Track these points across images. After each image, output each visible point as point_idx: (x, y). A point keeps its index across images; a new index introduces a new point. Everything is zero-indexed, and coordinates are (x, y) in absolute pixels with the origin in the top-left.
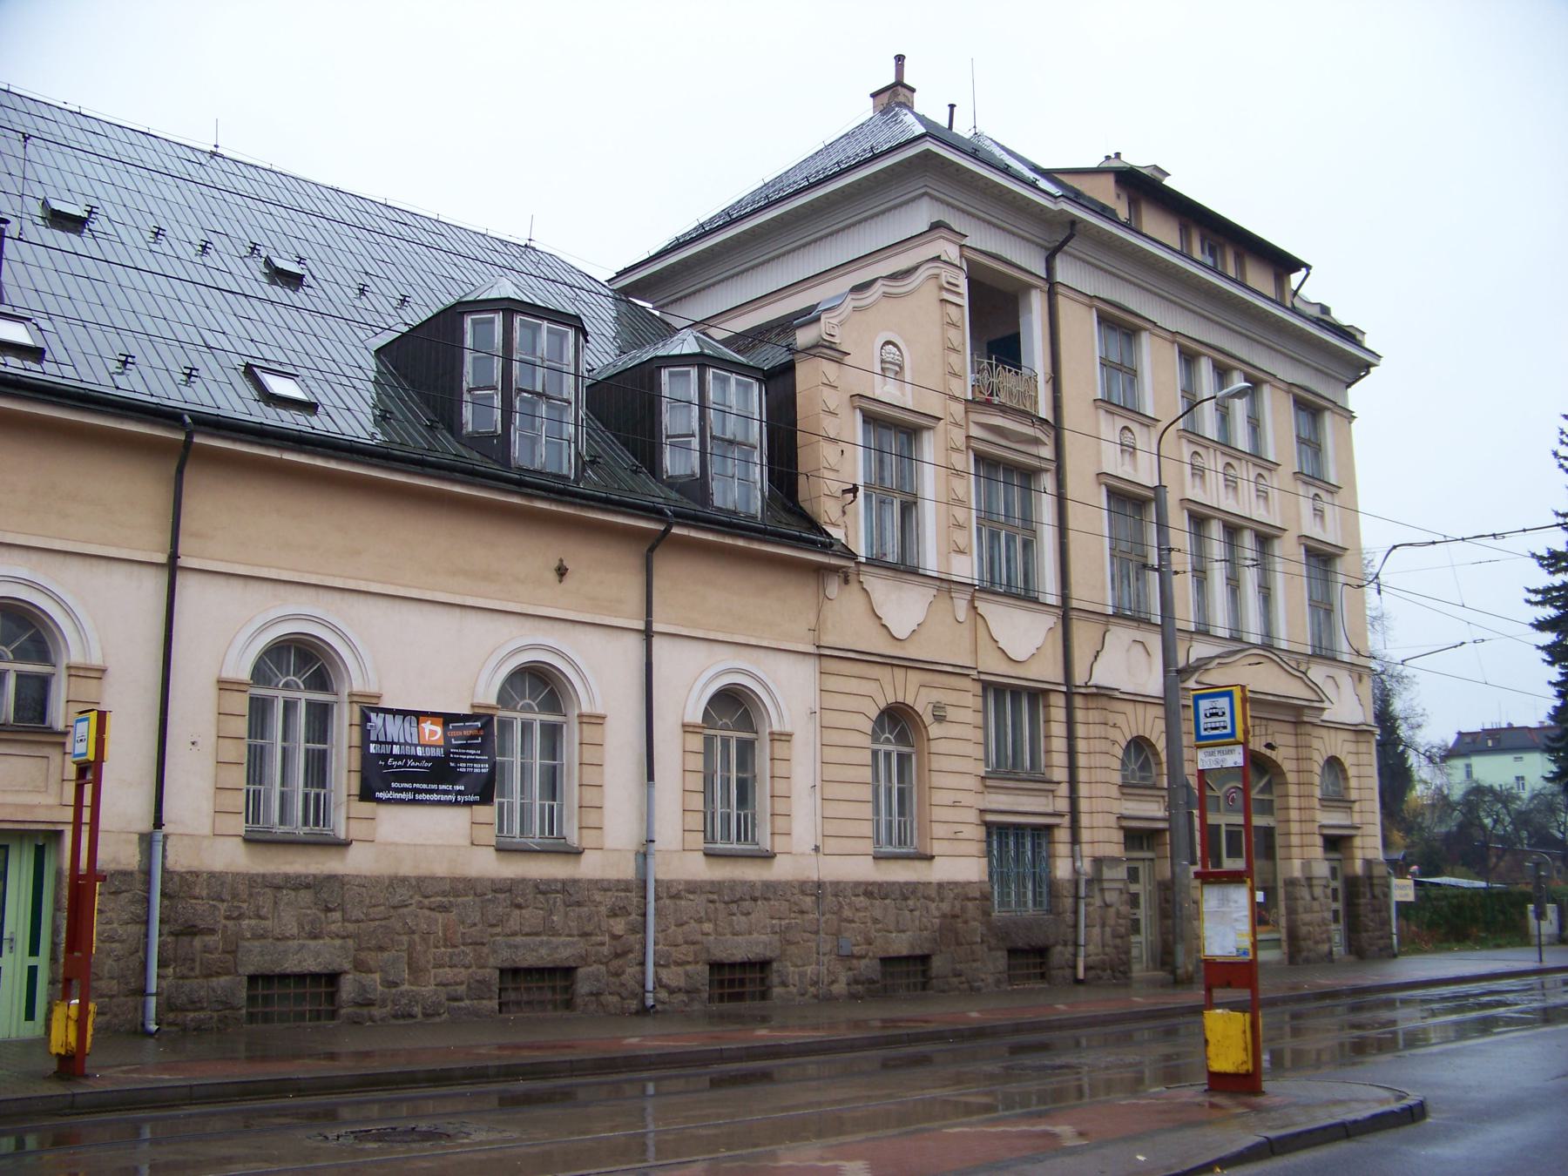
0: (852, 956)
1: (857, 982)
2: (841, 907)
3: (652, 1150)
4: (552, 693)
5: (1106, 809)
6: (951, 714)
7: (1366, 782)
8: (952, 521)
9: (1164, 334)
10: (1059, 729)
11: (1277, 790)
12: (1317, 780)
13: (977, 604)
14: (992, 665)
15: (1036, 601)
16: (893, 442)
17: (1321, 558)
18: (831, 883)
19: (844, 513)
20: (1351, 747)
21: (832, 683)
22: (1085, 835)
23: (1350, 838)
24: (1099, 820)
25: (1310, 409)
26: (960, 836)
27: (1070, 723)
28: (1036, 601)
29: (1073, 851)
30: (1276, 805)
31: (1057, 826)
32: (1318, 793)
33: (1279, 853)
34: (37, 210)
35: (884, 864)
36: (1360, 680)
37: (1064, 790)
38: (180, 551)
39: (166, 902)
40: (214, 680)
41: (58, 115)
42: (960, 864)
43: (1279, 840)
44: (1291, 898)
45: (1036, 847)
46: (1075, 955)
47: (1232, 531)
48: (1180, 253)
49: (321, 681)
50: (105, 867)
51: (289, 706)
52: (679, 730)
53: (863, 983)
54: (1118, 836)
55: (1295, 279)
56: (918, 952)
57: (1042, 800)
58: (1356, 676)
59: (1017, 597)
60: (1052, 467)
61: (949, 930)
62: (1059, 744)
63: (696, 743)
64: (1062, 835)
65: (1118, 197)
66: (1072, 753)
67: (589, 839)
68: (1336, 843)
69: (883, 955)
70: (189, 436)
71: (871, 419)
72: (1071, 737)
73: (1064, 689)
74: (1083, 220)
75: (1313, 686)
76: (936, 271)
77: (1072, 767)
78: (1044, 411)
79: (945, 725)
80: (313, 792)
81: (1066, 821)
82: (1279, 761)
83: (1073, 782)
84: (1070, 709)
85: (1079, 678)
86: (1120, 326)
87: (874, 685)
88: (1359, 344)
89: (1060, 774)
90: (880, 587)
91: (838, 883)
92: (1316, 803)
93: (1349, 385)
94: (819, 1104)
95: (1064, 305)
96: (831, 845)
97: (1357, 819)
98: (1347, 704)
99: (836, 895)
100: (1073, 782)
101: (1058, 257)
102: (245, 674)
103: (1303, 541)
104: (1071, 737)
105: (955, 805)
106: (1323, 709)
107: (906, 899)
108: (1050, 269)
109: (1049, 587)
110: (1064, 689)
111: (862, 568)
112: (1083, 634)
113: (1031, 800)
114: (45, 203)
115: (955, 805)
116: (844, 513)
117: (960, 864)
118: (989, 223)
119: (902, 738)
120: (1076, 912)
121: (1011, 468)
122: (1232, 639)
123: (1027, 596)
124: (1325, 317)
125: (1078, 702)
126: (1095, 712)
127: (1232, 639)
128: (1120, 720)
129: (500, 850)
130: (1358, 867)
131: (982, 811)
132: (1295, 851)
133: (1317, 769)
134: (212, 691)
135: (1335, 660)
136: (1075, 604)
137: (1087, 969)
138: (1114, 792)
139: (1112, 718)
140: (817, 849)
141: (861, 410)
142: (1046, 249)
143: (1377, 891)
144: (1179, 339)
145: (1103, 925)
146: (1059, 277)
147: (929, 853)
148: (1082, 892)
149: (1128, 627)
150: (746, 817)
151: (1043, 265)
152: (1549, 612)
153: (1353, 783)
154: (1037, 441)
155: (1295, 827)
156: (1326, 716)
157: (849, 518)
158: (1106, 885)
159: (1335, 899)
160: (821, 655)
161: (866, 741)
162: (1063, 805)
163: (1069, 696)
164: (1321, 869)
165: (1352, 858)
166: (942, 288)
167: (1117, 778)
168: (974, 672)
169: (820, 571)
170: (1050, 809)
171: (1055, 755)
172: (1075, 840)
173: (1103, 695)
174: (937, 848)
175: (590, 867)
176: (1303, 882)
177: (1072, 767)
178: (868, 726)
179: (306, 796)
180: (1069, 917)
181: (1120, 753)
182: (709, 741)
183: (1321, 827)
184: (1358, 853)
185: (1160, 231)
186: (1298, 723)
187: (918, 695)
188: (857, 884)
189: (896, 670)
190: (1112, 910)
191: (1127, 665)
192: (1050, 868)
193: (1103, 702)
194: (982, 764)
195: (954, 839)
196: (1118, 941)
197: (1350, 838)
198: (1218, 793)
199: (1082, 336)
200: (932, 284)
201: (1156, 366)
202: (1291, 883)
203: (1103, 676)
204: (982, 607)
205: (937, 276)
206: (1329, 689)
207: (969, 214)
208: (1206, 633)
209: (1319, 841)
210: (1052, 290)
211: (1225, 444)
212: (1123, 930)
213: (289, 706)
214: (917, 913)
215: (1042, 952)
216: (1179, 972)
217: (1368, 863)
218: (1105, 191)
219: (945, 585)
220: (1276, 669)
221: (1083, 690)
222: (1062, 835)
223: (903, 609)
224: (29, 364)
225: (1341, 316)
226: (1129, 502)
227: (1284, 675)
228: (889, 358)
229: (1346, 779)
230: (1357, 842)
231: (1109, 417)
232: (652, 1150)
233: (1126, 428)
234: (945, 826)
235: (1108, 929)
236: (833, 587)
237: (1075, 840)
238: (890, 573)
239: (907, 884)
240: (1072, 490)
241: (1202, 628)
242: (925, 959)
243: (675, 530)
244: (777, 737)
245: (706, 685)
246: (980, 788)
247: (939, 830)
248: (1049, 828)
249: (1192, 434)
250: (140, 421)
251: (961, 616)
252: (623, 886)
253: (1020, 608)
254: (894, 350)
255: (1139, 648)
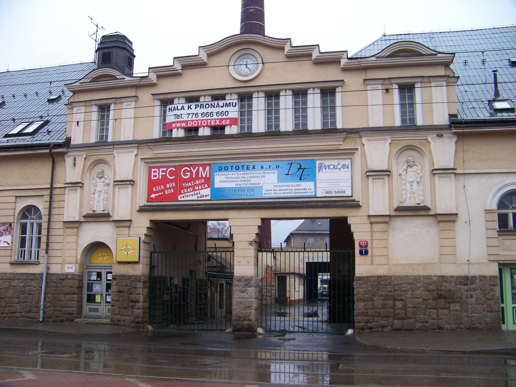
3: (39, 364)
34: (507, 63)
40: (483, 209)
41: (511, 30)
50: (77, 270)
51: (32, 224)
80: (37, 249)
94: (373, 371)
102: (494, 207)
114: (509, 60)
134: (483, 214)
179: (35, 251)
213: (32, 224)
224: (510, 114)
232: (39, 364)
243: (48, 151)
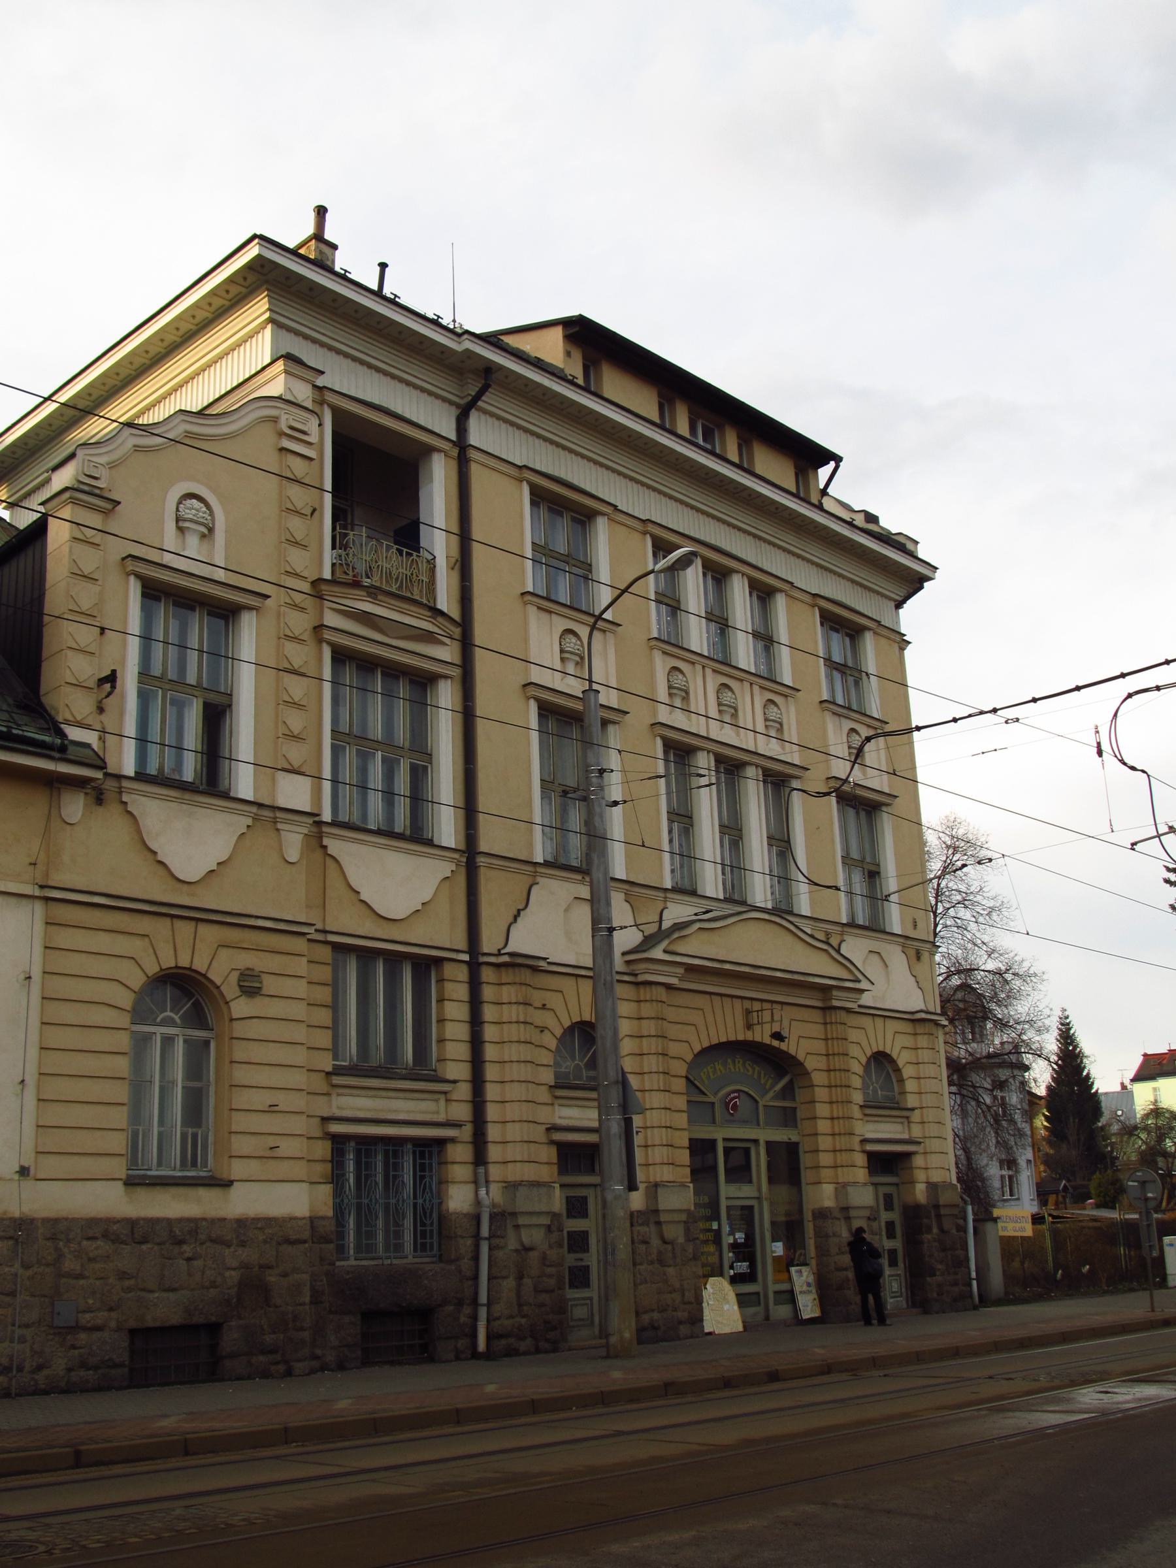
0: (76, 1328)
1: (84, 1365)
2: (60, 1256)
4: (197, 1006)
5: (527, 1114)
6: (270, 985)
7: (931, 1085)
8: (282, 730)
9: (630, 521)
10: (457, 1011)
11: (801, 1095)
12: (857, 1082)
13: (326, 841)
14: (346, 922)
15: (430, 843)
16: (197, 629)
17: (862, 806)
18: (46, 1221)
19: (101, 710)
20: (908, 1041)
21: (65, 938)
22: (494, 1153)
23: (908, 1155)
24: (514, 1132)
25: (843, 625)
26: (278, 1153)
27: (475, 1003)
28: (884, 932)
29: (475, 1174)
30: (800, 1114)
31: (453, 1140)
32: (858, 1097)
33: (806, 1176)
35: (142, 1193)
36: (918, 958)
37: (464, 1091)
39: (961, 1222)
42: (279, 1191)
43: (805, 1160)
44: (820, 1235)
45: (421, 1172)
46: (475, 1318)
47: (731, 767)
48: (796, 496)
51: (168, 1041)
53: (96, 1368)
54: (551, 1153)
55: (824, 472)
56: (198, 1319)
57: (899, 1127)
58: (912, 953)
59: (400, 837)
60: (456, 672)
61: (254, 1287)
62: (458, 1031)
64: (460, 1153)
65: (568, 354)
66: (476, 1042)
68: (888, 1163)
69: (132, 1324)
71: (153, 592)
72: (476, 1021)
73: (466, 957)
74: (501, 368)
75: (847, 963)
76: (274, 412)
77: (477, 1062)
78: (446, 600)
79: (258, 1000)
81: (466, 1133)
82: (801, 1057)
83: (478, 1081)
84: (475, 985)
85: (489, 942)
86: (568, 509)
87: (138, 943)
88: (913, 555)
89: (458, 1070)
90: (157, 814)
91: (56, 1221)
92: (856, 1112)
93: (899, 605)
95: (477, 473)
96: (51, 1166)
97: (916, 1132)
98: (895, 986)
99: (53, 1238)
100: (478, 1081)
101: (474, 415)
103: (131, 565)
104: (476, 1021)
105: (272, 1109)
106: (863, 991)
107: (181, 1242)
108: (462, 430)
109: (447, 827)
110: (466, 957)
111: (325, 829)
112: (496, 890)
113: (411, 1105)
115: (272, 1109)
116: (101, 710)
117: (279, 1191)
118: (370, 366)
120: (476, 1258)
121: (393, 672)
122: (727, 900)
123: (418, 836)
124: (871, 527)
125: (487, 974)
126: (512, 989)
127: (727, 900)
128: (554, 1001)
129: (131, 1183)
130: (920, 1192)
131: (325, 1120)
132: (826, 1174)
133: (857, 1068)
135: (884, 932)
136: (483, 846)
137: (489, 1338)
138: (544, 1095)
139: (537, 997)
140: (24, 1171)
141: (537, 699)
142: (458, 406)
143: (948, 1224)
144: (651, 528)
145: (520, 1277)
146: (474, 439)
147: (225, 1176)
148: (485, 1231)
149: (567, 880)
150: (195, 1136)
151: (453, 425)
153: (910, 1086)
154: (428, 637)
155: (825, 1143)
156: (866, 999)
157: (108, 720)
158: (521, 1221)
159: (891, 1235)
160: (47, 899)
161: (124, 1020)
162: (462, 1112)
163: (474, 967)
164: (863, 1197)
165: (912, 1182)
166: (282, 434)
167: (548, 1077)
168: (311, 930)
169: (54, 784)
170: (441, 1118)
171: (449, 1046)
172: (480, 1158)
173: (525, 966)
174: (238, 1169)
176: (837, 1214)
177: (477, 1062)
178: (125, 999)
179: (182, 1134)
180: (466, 1264)
181: (553, 1044)
183: (864, 1141)
184: (920, 1176)
185: (626, 402)
186: (827, 1009)
187: (217, 959)
188: (93, 1222)
189: (179, 924)
190: (534, 1255)
191: (551, 926)
192: (440, 1198)
193: (526, 976)
194: (330, 1055)
195: (271, 1155)
196: (545, 1298)
197: (908, 1155)
198: (712, 1099)
199: (509, 520)
200: (267, 431)
201: (610, 554)
202: (821, 1214)
203: (523, 941)
204: (335, 846)
205: (275, 420)
206: (872, 968)
207: (339, 352)
208: (693, 893)
209: (860, 1159)
210: (462, 452)
211: (722, 661)
212: (552, 1282)
214: (198, 1263)
215: (423, 1315)
216: (613, 1340)
217: (932, 1187)
218: (552, 347)
219: (267, 813)
220: (789, 938)
221: (492, 959)
222: (460, 1153)
223: (193, 842)
225: (890, 523)
226: (567, 721)
227: (800, 946)
228: (189, 515)
229: (901, 1081)
230: (918, 1161)
231: (836, 718)
233: (853, 730)
234: (253, 1140)
235: (527, 1281)
236: (74, 806)
237: (480, 1158)
238: (173, 793)
239: (180, 1220)
240: (484, 703)
241: (686, 885)
242: (214, 1329)
246: (324, 1088)
247: (241, 1145)
248: (441, 1142)
249: (671, 643)
251: (293, 855)
253: (398, 850)
254: (574, 640)
255: (876, 958)
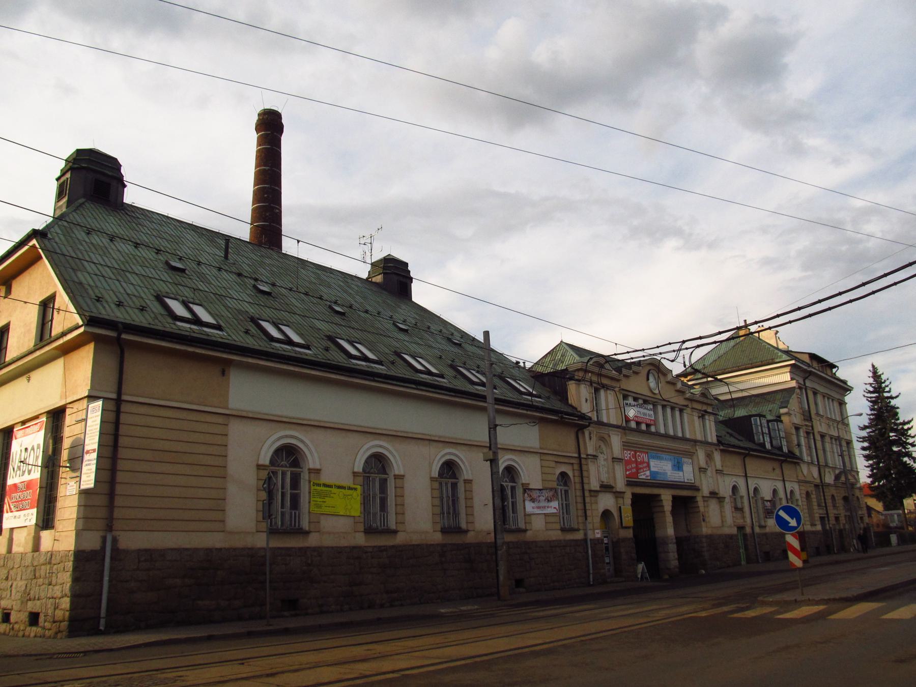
38: (123, 391)
49: (296, 463)
51: (284, 474)
52: (255, 469)
55: (834, 370)
63: (436, 485)
67: (400, 527)
70: (120, 335)
119: (566, 484)
152: (866, 444)
175: (470, 538)
182: (441, 484)
244: (397, 477)
245: (274, 443)
250: (99, 327)
252: (581, 540)
